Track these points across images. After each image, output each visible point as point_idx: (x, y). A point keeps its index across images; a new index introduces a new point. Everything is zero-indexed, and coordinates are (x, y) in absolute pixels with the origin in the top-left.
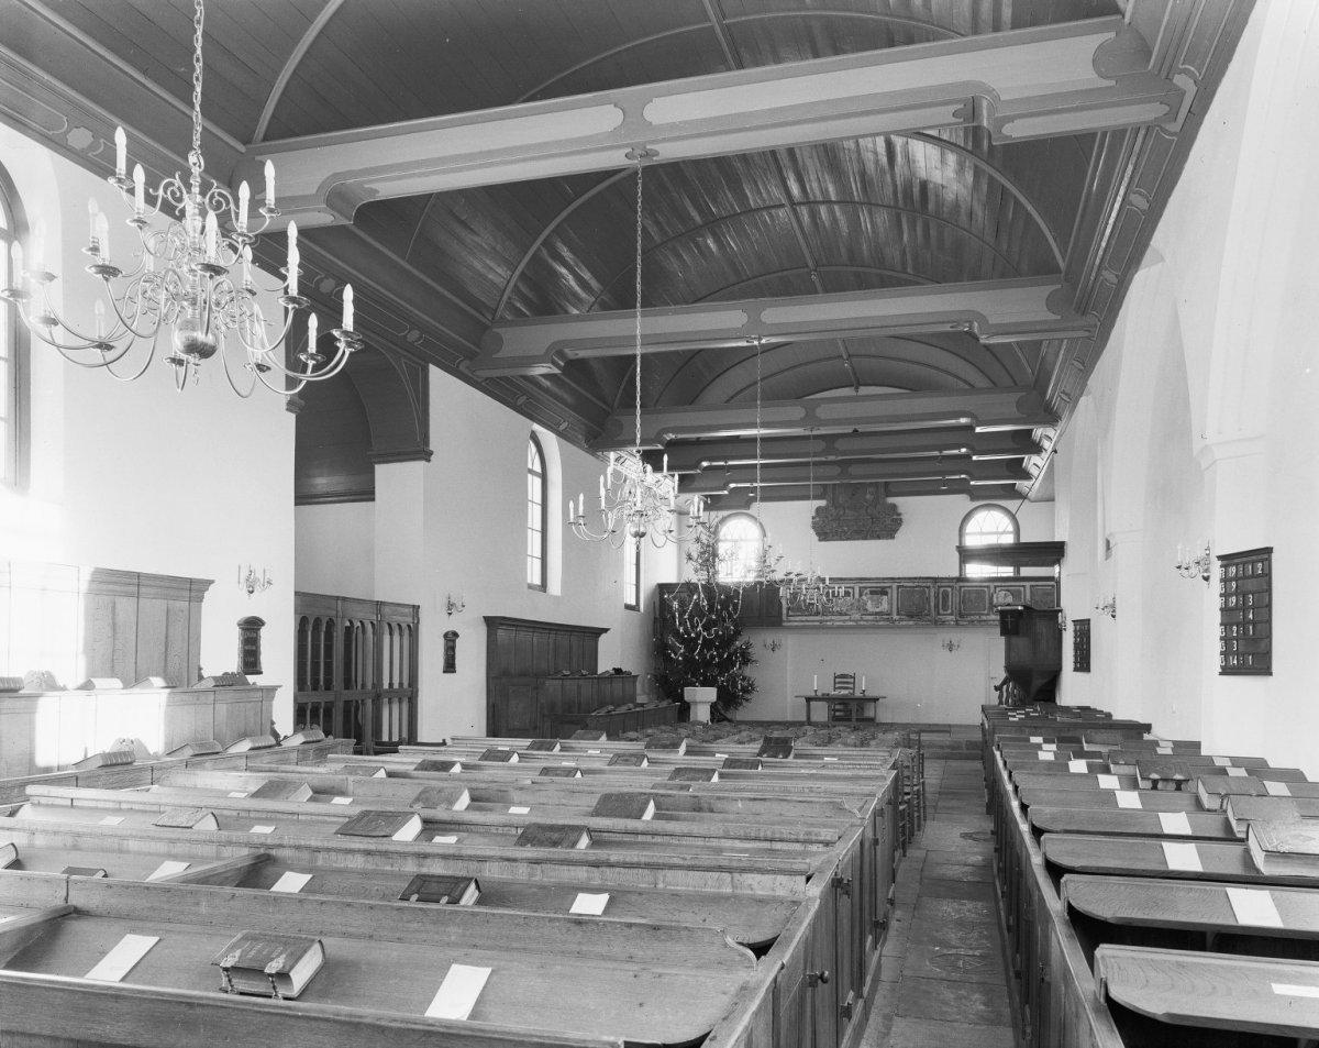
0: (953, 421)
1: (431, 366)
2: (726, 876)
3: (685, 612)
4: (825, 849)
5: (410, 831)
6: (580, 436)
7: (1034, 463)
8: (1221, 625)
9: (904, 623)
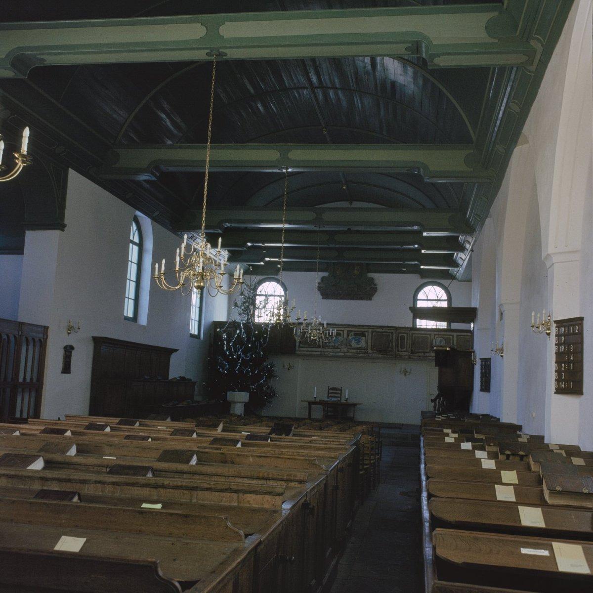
0: (410, 228)
1: (70, 169)
2: (235, 495)
3: (231, 341)
4: (299, 485)
5: (38, 465)
6: (167, 221)
7: (462, 258)
8: (556, 363)
9: (376, 355)
